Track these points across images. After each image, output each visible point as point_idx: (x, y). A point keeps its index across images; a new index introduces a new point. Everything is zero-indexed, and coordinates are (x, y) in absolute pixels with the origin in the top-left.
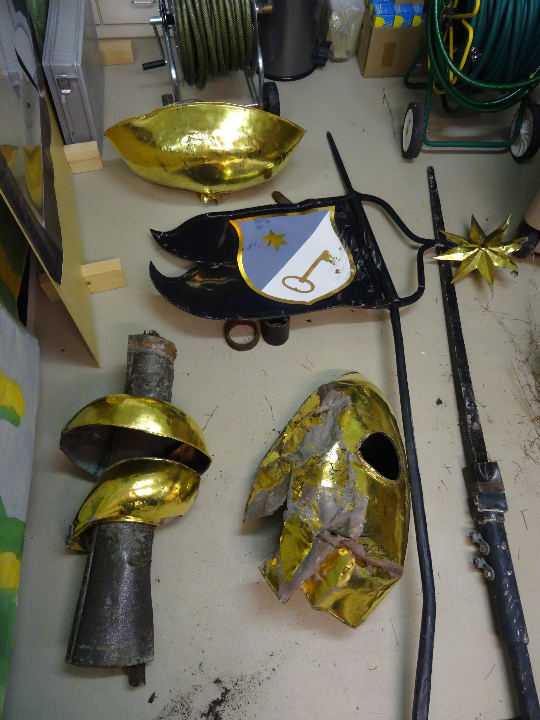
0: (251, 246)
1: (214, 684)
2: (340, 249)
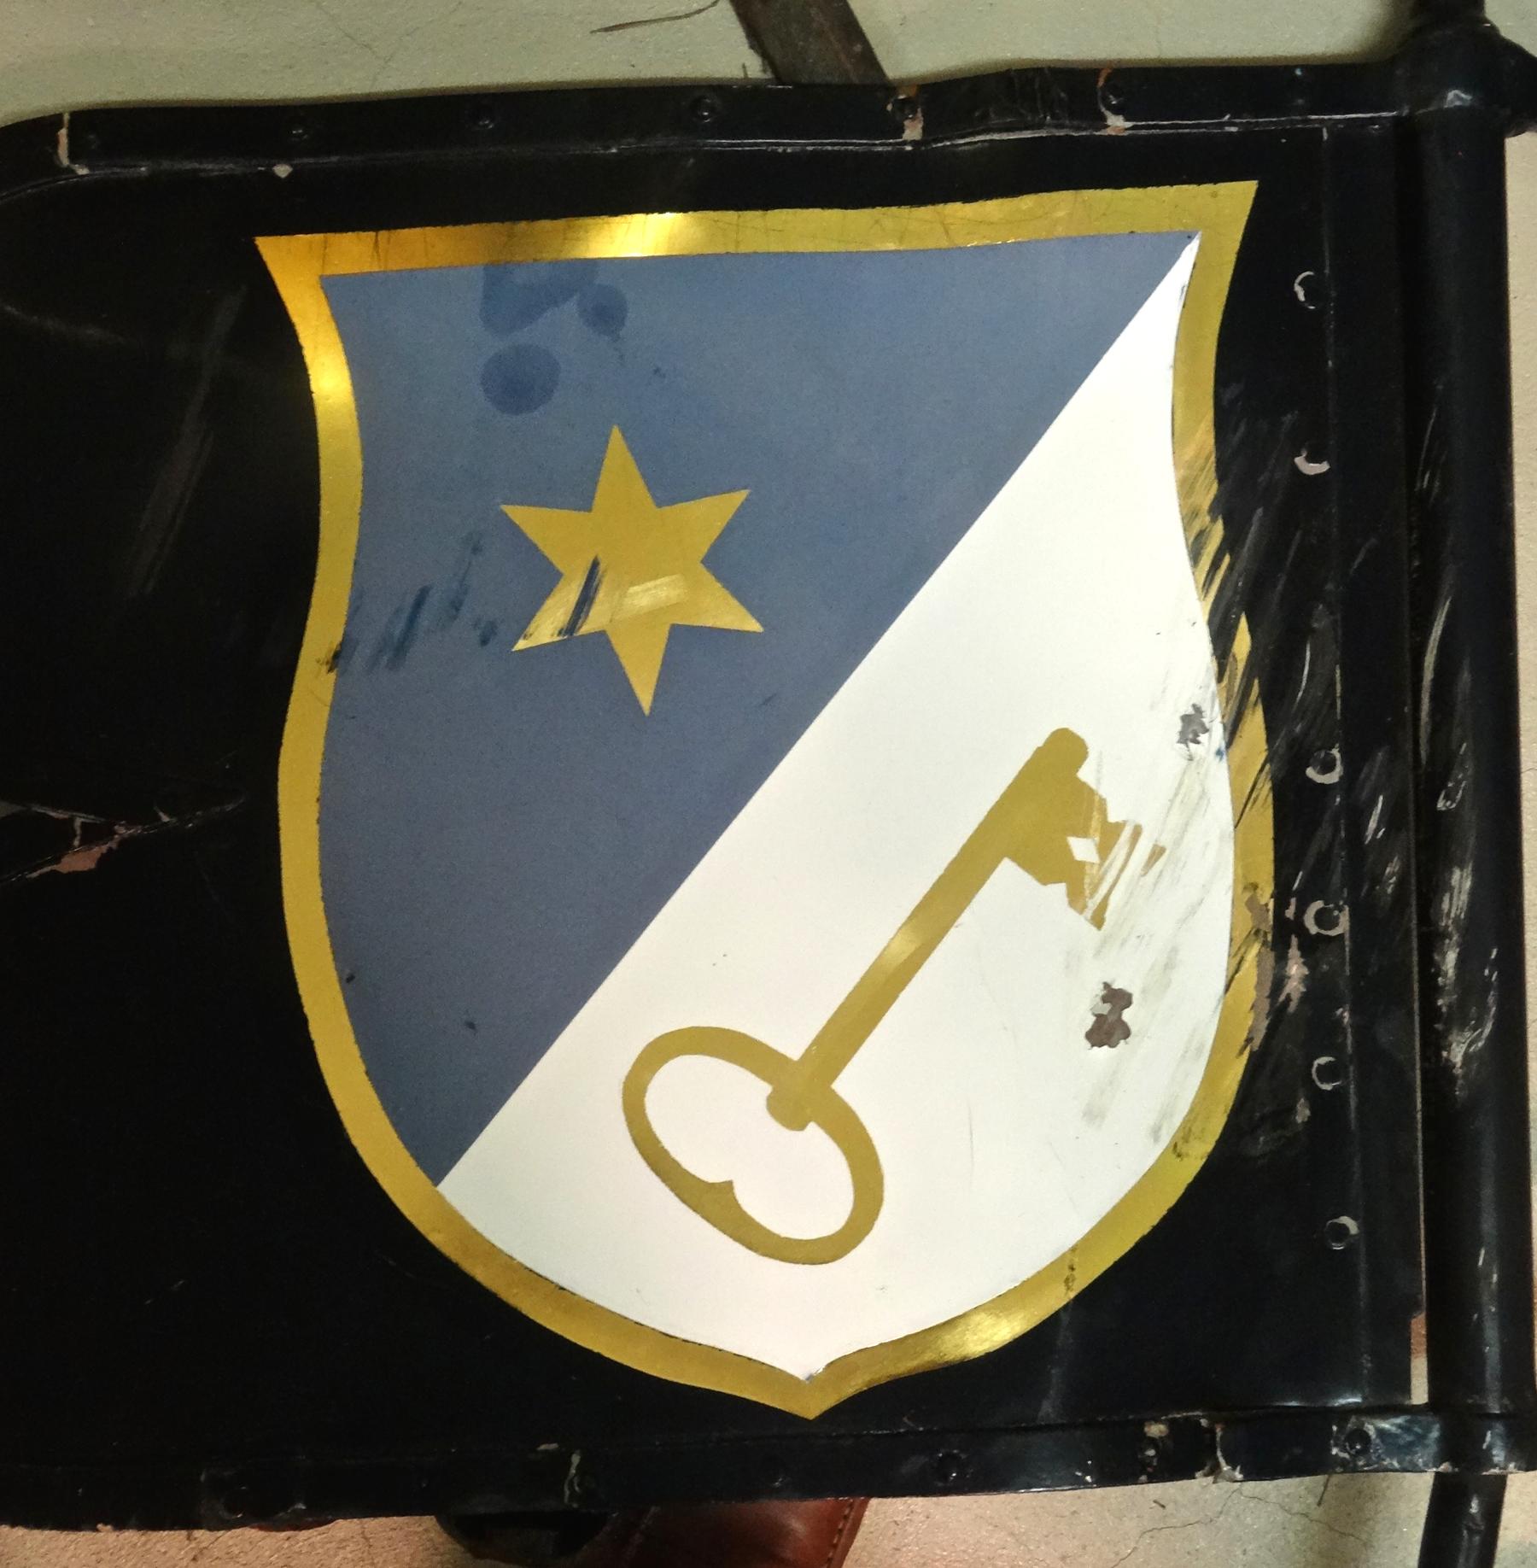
0: (412, 620)
1: (1102, 986)
2: (1192, 726)
